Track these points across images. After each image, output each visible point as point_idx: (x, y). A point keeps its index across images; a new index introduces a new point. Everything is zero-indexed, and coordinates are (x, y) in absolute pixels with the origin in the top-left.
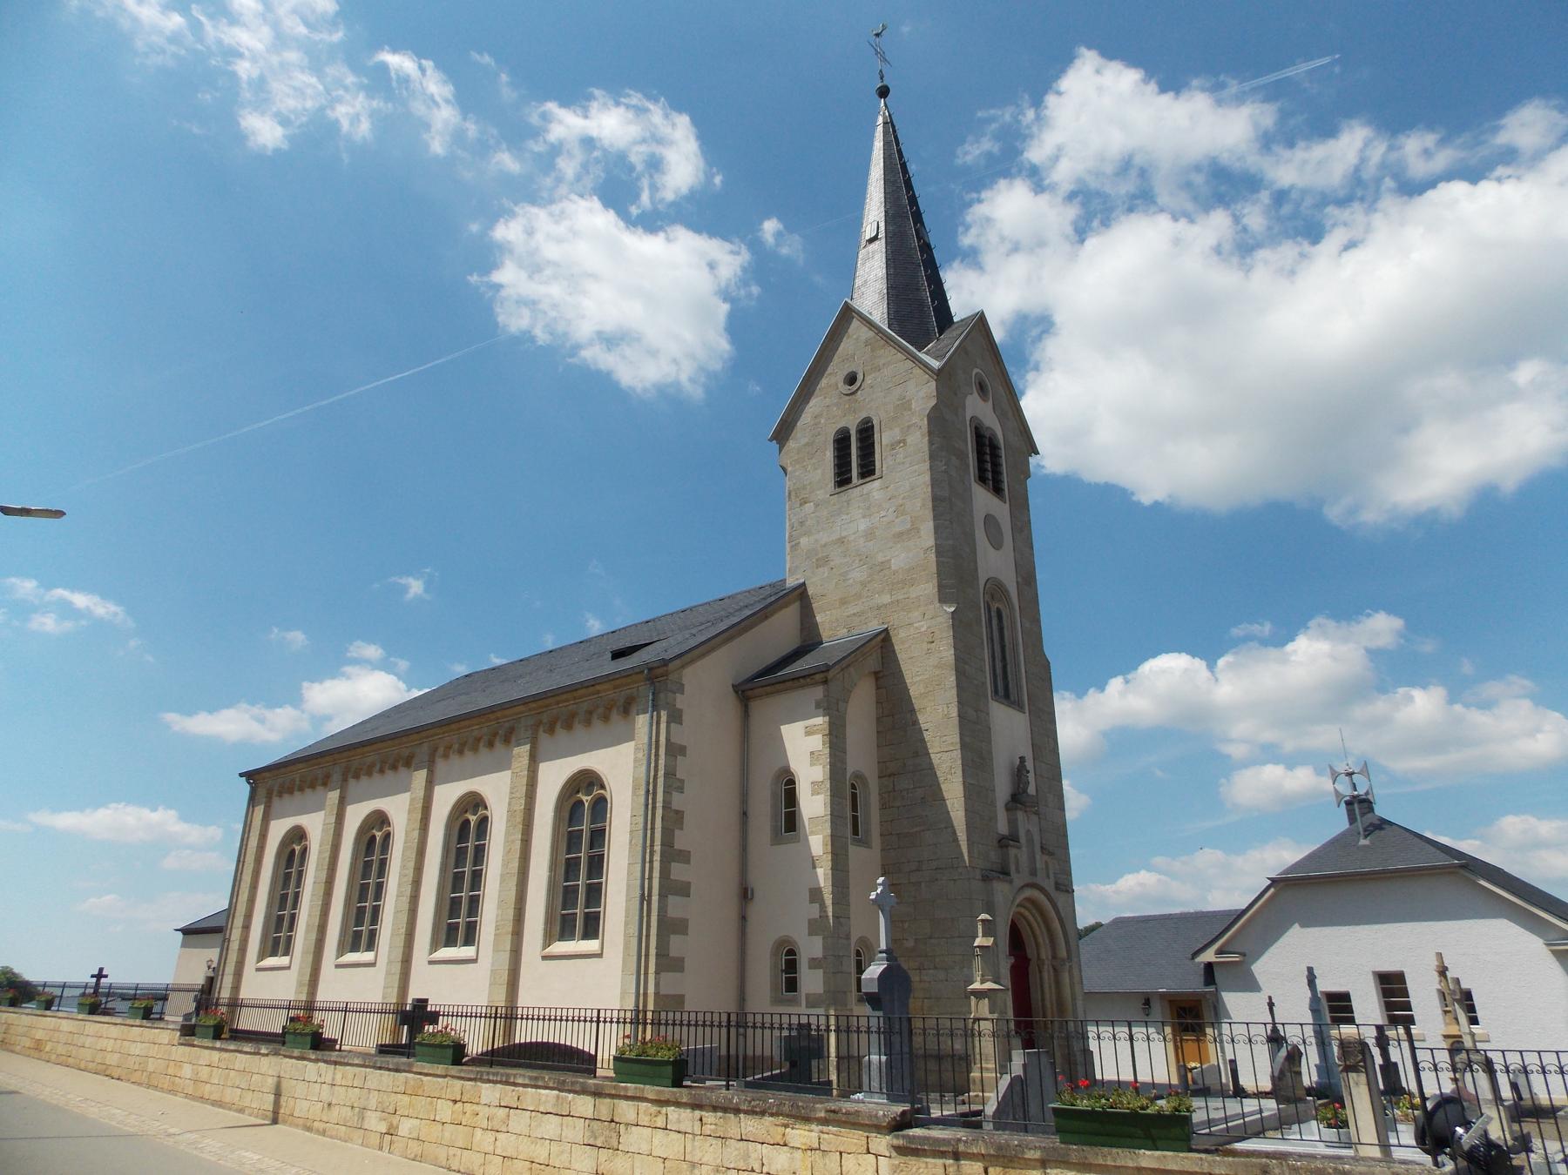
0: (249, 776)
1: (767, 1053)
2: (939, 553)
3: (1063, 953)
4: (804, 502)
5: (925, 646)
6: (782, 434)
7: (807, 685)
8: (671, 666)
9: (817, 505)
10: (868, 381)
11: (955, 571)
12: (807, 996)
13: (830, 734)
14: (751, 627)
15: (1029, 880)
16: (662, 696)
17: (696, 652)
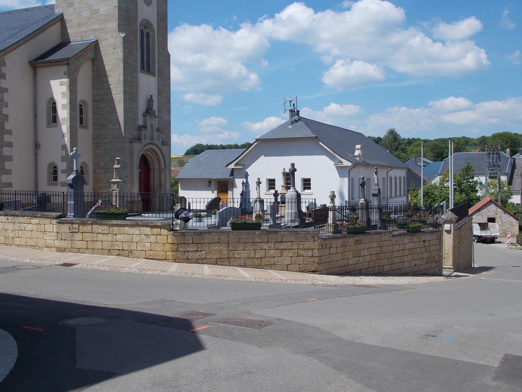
1: (27, 202)
2: (120, 10)
3: (163, 167)
5: (112, 50)
12: (61, 182)
13: (70, 86)
15: (149, 141)
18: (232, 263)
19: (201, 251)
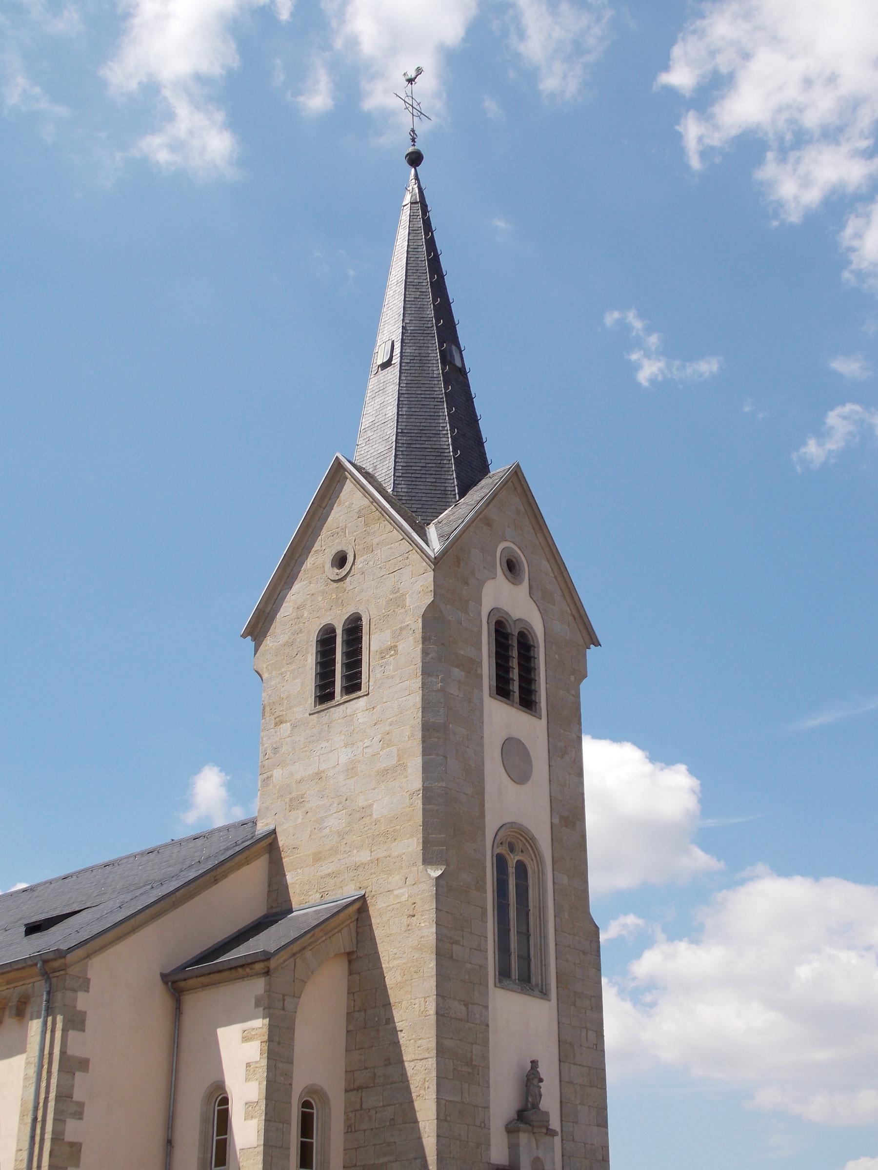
4: (279, 722)
5: (405, 920)
6: (259, 627)
7: (248, 976)
8: (70, 958)
9: (294, 727)
10: (359, 564)
11: (448, 816)
13: (270, 1040)
14: (192, 896)
16: (59, 995)
17: (139, 917)
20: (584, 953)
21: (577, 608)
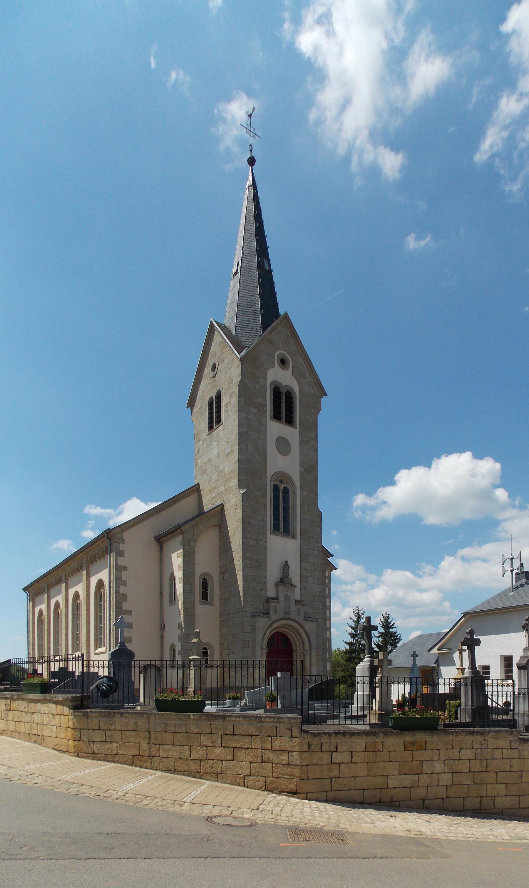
0: (25, 589)
5: (234, 511)
6: (191, 404)
9: (203, 441)
11: (250, 469)
15: (283, 616)
18: (155, 764)
19: (111, 742)
20: (314, 522)
21: (316, 379)
